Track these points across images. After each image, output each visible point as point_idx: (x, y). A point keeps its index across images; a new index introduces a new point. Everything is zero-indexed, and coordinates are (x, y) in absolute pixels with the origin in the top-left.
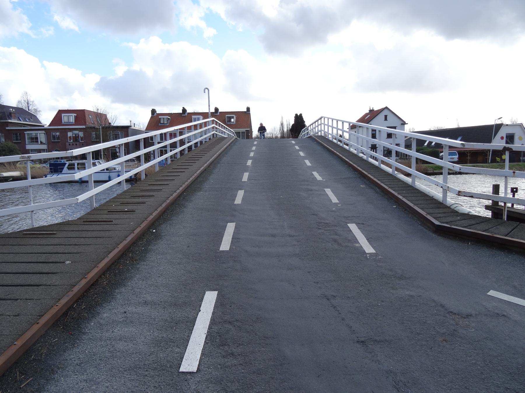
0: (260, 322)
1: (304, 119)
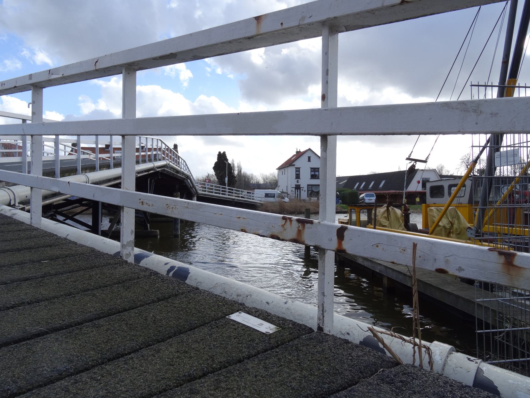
0: (204, 393)
1: (227, 157)
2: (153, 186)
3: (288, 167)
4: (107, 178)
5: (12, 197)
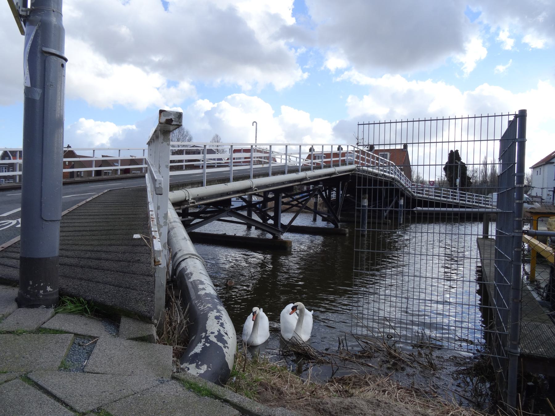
2: (345, 188)
3: (544, 165)
4: (273, 183)
5: (187, 195)
